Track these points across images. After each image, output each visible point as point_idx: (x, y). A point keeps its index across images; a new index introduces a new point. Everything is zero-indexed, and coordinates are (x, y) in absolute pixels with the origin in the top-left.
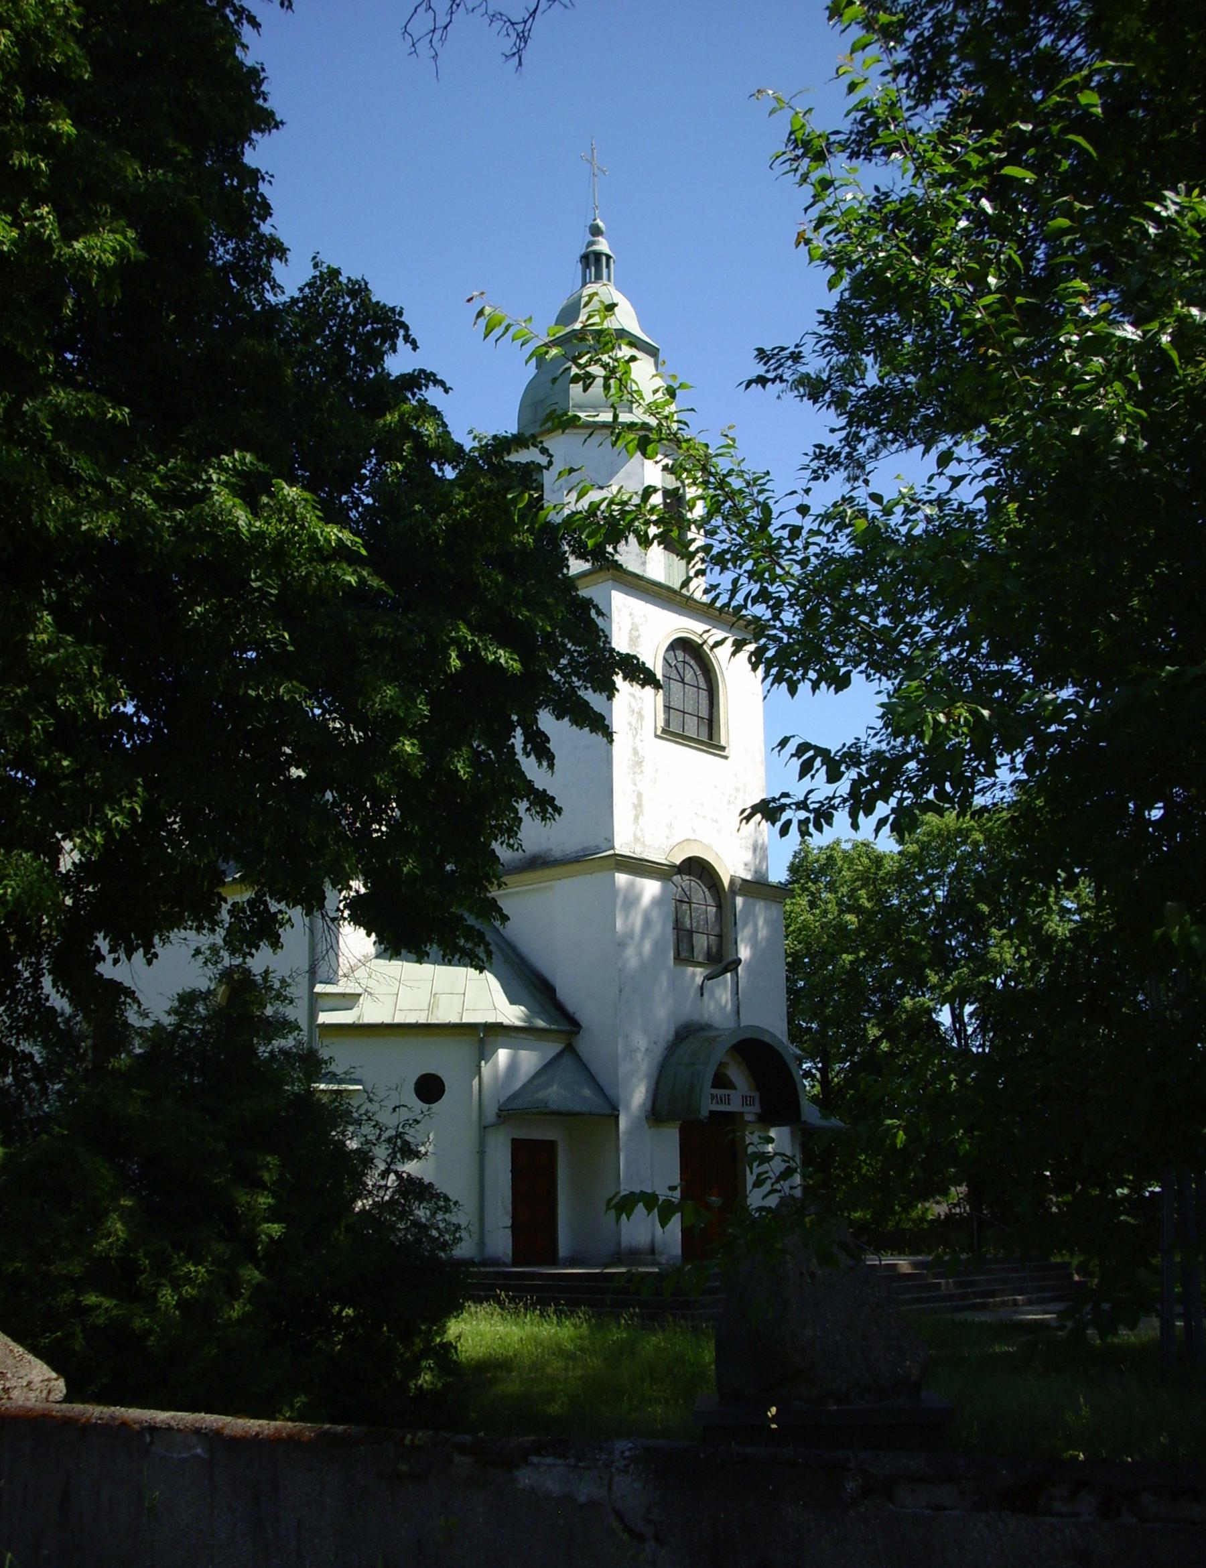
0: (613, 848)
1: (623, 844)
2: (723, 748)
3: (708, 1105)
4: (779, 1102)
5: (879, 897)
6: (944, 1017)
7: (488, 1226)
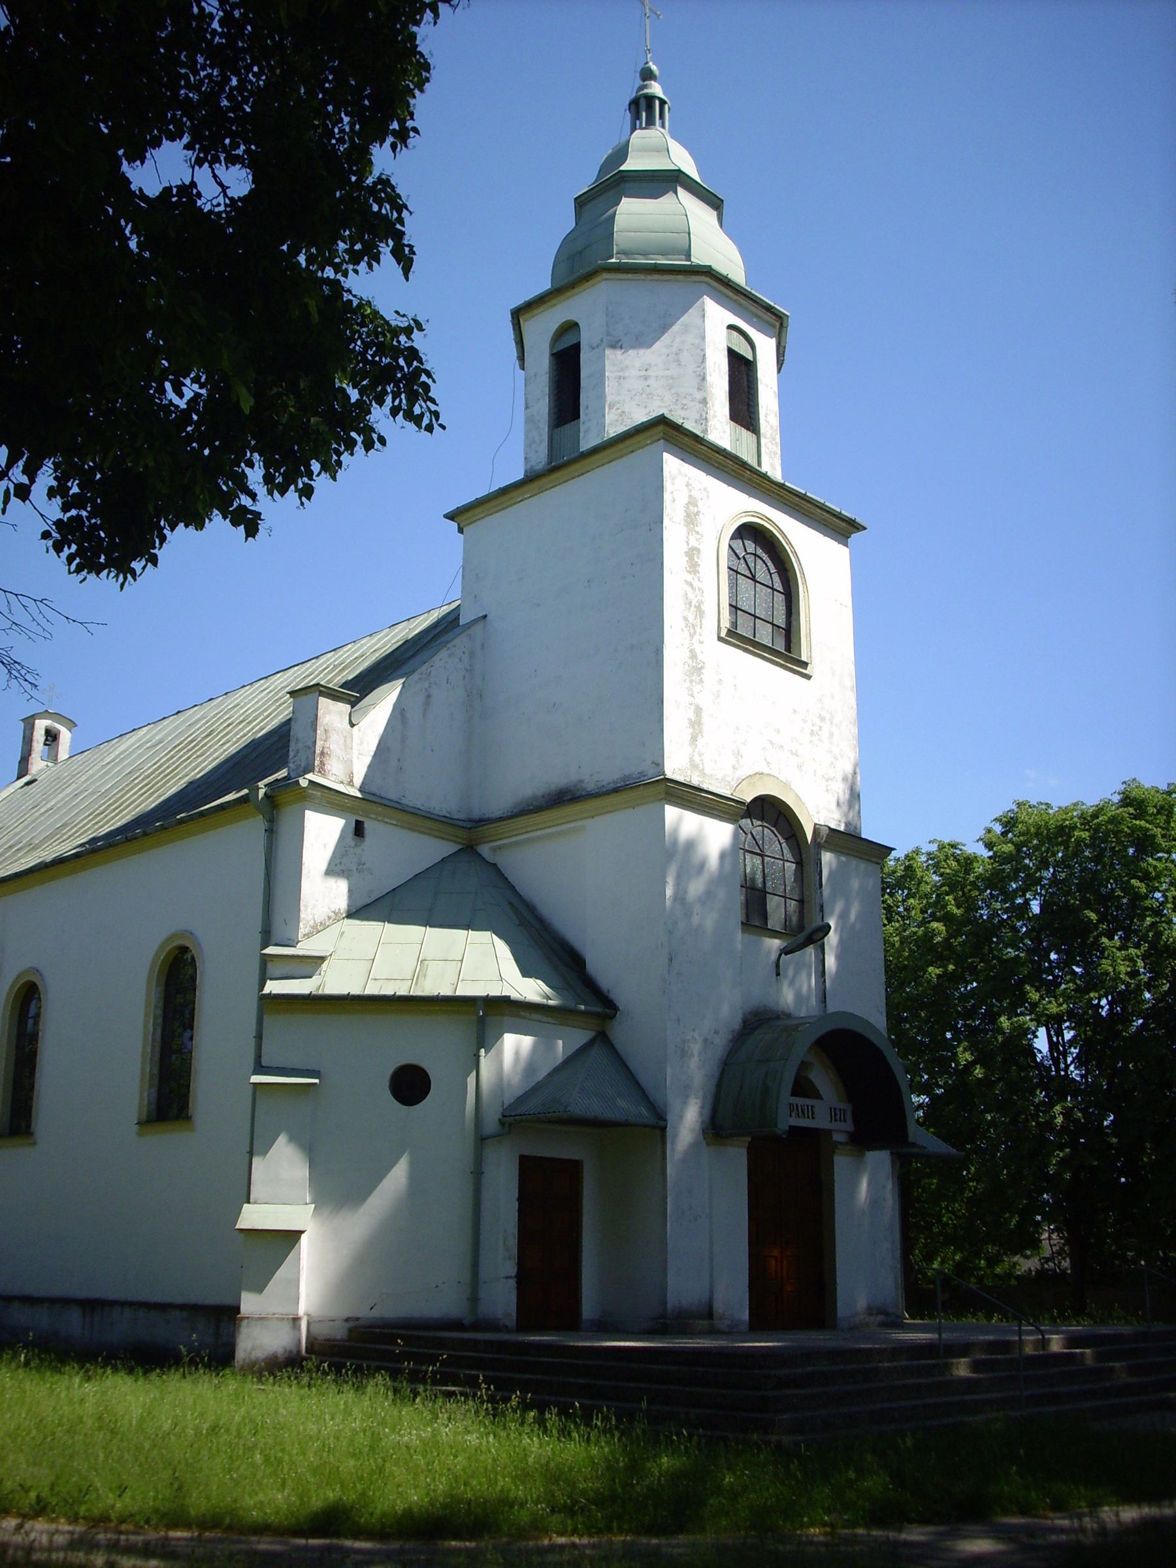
0: (664, 774)
1: (675, 766)
2: (805, 665)
3: (786, 1121)
4: (877, 1124)
5: (969, 905)
6: (1041, 1043)
7: (483, 1275)
